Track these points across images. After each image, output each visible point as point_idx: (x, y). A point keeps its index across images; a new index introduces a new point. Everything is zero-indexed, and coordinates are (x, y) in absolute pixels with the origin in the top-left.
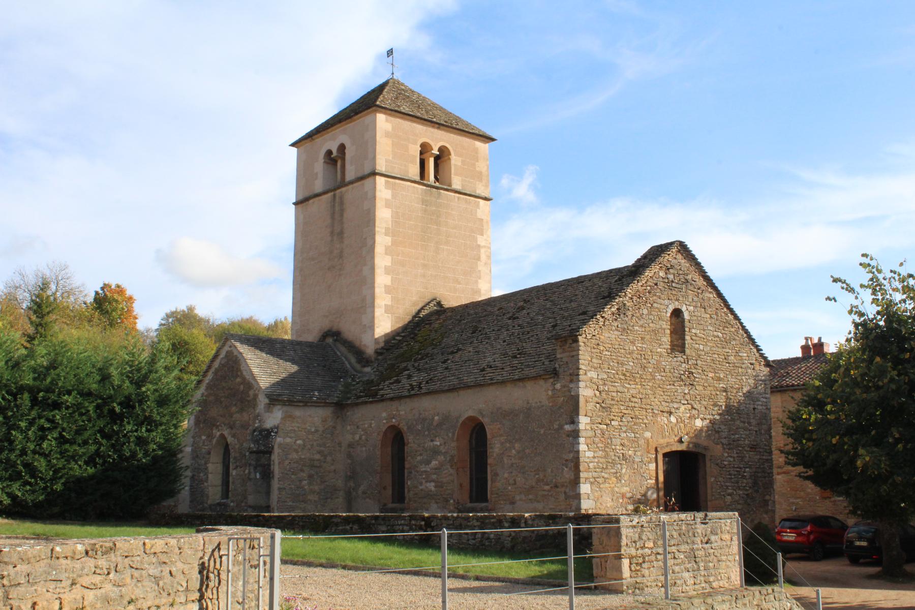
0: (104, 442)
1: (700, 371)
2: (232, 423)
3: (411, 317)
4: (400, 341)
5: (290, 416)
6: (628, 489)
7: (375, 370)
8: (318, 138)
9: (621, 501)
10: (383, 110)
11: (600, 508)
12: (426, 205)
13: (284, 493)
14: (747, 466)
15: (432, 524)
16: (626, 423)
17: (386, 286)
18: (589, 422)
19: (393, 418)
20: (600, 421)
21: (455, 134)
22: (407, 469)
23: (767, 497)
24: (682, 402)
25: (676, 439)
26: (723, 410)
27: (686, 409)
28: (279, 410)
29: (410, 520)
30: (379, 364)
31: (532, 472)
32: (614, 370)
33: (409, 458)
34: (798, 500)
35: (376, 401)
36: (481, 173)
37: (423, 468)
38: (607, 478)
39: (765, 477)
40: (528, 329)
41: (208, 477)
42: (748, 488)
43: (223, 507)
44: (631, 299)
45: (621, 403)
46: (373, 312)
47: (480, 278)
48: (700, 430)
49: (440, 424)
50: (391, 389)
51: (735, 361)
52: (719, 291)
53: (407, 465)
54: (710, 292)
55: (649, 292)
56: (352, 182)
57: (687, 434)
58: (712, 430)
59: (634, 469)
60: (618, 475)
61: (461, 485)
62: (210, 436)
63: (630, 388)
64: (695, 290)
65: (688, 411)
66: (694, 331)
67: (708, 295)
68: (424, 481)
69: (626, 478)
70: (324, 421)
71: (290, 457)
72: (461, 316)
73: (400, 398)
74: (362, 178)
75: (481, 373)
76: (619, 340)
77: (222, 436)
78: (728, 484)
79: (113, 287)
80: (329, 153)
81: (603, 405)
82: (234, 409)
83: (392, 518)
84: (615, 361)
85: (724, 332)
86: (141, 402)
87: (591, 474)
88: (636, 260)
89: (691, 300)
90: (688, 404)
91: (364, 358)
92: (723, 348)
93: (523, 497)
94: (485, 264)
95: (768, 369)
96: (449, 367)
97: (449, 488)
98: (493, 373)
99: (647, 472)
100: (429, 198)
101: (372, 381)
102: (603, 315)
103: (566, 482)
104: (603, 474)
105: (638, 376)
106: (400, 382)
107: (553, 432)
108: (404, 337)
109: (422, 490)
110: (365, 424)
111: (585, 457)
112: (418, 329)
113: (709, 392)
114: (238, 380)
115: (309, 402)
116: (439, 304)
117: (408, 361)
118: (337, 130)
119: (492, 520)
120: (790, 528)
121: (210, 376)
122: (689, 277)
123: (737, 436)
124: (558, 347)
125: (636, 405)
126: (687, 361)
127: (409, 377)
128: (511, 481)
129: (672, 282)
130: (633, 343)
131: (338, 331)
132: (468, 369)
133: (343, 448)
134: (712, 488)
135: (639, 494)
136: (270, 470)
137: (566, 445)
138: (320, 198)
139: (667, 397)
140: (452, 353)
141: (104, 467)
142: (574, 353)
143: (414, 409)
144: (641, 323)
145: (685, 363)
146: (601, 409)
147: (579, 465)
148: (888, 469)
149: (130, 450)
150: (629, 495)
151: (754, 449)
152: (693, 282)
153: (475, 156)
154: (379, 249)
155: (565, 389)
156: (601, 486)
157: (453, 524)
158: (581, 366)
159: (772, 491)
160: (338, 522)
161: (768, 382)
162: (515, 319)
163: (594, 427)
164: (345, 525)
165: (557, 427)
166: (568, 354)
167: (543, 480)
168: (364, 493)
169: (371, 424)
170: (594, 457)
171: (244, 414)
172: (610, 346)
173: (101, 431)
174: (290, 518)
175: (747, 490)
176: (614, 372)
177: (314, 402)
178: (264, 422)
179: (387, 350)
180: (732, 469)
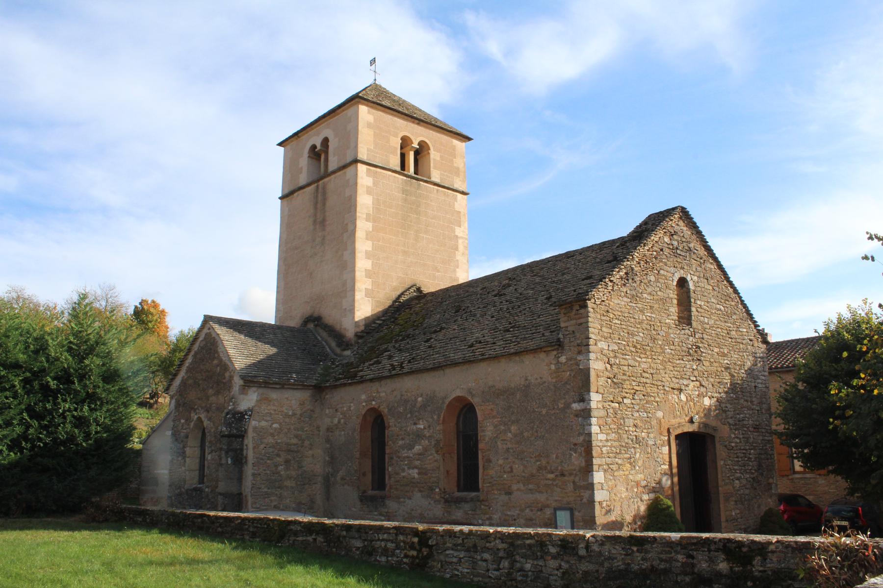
0: (35, 423)
2: (208, 406)
3: (391, 302)
4: (380, 324)
5: (266, 399)
7: (355, 353)
8: (304, 134)
9: (636, 490)
10: (366, 102)
12: (406, 195)
14: (752, 447)
15: (430, 543)
18: (601, 399)
19: (374, 400)
20: (612, 399)
22: (388, 454)
23: (771, 480)
24: (692, 378)
25: (687, 419)
26: (729, 388)
27: (694, 386)
28: (255, 392)
29: (397, 535)
30: (359, 347)
31: (531, 458)
32: (625, 341)
33: (390, 442)
35: (355, 383)
36: (458, 169)
37: (405, 453)
38: (621, 465)
39: (768, 459)
40: (519, 303)
41: (185, 461)
42: (753, 471)
43: (198, 492)
44: (639, 263)
45: (633, 378)
46: (354, 295)
47: (458, 268)
49: (424, 406)
50: (371, 370)
51: (737, 336)
52: (719, 262)
53: (387, 451)
55: (656, 258)
56: (334, 172)
58: (719, 410)
60: (632, 461)
61: (448, 472)
62: (188, 420)
63: (641, 362)
64: (698, 259)
65: (696, 389)
66: (699, 302)
67: (709, 265)
68: (406, 468)
69: (640, 463)
70: (302, 404)
71: (266, 441)
72: (442, 299)
73: (380, 379)
74: (344, 167)
75: (469, 349)
76: (628, 307)
77: (199, 419)
78: (736, 467)
79: (149, 302)
80: (314, 147)
81: (614, 380)
82: (211, 391)
83: (371, 530)
84: (625, 331)
86: (82, 378)
88: (635, 227)
89: (694, 270)
90: (697, 381)
91: (344, 342)
92: (725, 322)
93: (521, 486)
94: (463, 254)
95: (765, 346)
96: (433, 346)
97: (434, 475)
98: (484, 348)
99: (661, 456)
100: (409, 188)
101: (352, 363)
102: (611, 279)
103: (575, 470)
104: (617, 459)
105: (649, 348)
106: (380, 363)
107: (558, 411)
108: (384, 321)
109: (404, 477)
110: (344, 407)
111: (597, 440)
112: (398, 314)
114: (215, 362)
115: (285, 384)
116: (419, 290)
117: (389, 343)
118: (321, 126)
119: (528, 542)
121: (190, 360)
122: (692, 245)
124: (562, 315)
125: (648, 381)
126: (693, 335)
127: (390, 357)
128: (507, 469)
129: (677, 248)
130: (642, 311)
131: (319, 316)
132: (454, 346)
133: (321, 433)
135: (653, 482)
136: (242, 455)
137: (574, 426)
139: (677, 373)
140: (435, 332)
141: (32, 453)
142: (582, 320)
143: (395, 390)
144: (649, 290)
145: (692, 336)
146: (612, 384)
147: (591, 450)
149: (66, 433)
150: (644, 483)
152: (696, 251)
153: (453, 153)
154: (360, 234)
155: (571, 362)
156: (616, 474)
157: (463, 545)
158: (591, 335)
160: (297, 531)
161: (765, 360)
162: (501, 295)
163: (606, 404)
164: (307, 536)
165: (562, 406)
166: (573, 322)
167: (546, 468)
168: (343, 479)
169: (350, 407)
170: (607, 441)
171: (220, 396)
172: (620, 314)
173: (30, 410)
174: (240, 521)
175: (753, 473)
176: (624, 343)
177: (294, 385)
178: (238, 405)
179: (367, 333)
180: (739, 451)
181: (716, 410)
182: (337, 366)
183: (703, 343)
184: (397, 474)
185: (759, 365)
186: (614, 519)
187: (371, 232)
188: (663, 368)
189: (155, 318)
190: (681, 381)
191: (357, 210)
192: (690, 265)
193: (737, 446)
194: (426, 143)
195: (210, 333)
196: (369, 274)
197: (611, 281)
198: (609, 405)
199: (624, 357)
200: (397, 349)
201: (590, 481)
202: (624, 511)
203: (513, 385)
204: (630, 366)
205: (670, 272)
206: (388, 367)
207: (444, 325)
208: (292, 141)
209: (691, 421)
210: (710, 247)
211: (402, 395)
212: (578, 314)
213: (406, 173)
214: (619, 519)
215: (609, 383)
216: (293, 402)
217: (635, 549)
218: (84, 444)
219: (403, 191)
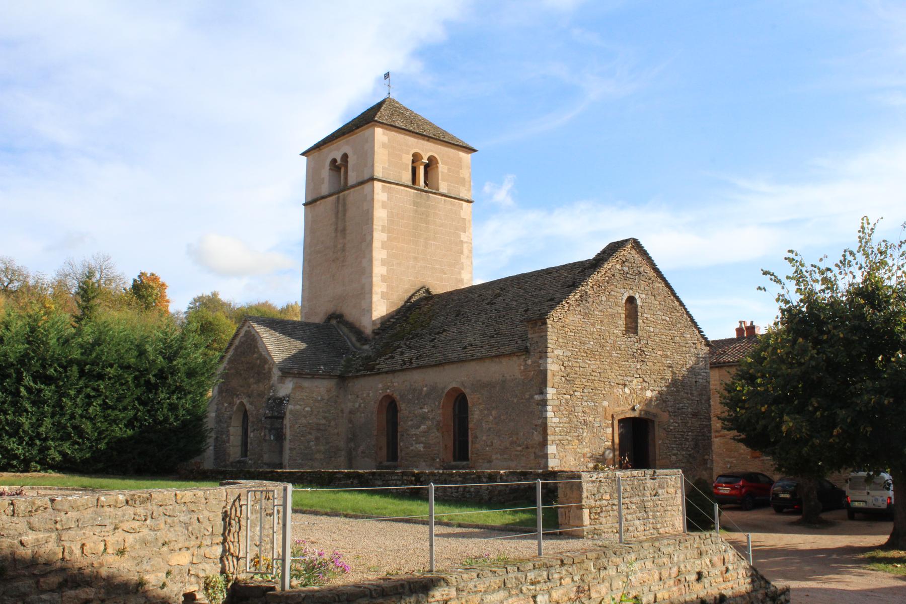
0: (141, 408)
1: (650, 350)
4: (394, 322)
8: (325, 148)
9: (582, 460)
10: (381, 125)
12: (417, 207)
15: (421, 479)
18: (555, 392)
19: (388, 389)
23: (706, 457)
24: (635, 376)
25: (630, 407)
26: (670, 383)
27: (638, 382)
28: (290, 381)
29: (402, 476)
33: (402, 423)
37: (413, 431)
38: (571, 441)
39: (704, 440)
40: (504, 313)
44: (592, 287)
46: (371, 298)
47: (463, 270)
51: (680, 341)
53: (399, 429)
55: (607, 282)
56: (353, 187)
58: (659, 400)
59: (594, 433)
61: (446, 446)
62: (231, 404)
65: (639, 384)
66: (645, 315)
68: (414, 443)
70: (329, 391)
71: (300, 421)
73: (393, 372)
76: (581, 322)
77: (242, 404)
78: (674, 446)
79: (148, 275)
81: (567, 378)
82: (252, 380)
84: (578, 341)
89: (643, 289)
91: (363, 337)
93: (498, 456)
99: (605, 435)
103: (535, 444)
105: (598, 353)
106: (394, 358)
108: (397, 319)
109: (412, 450)
111: (552, 422)
115: (316, 375)
116: (428, 291)
119: (472, 476)
120: (725, 483)
121: (231, 352)
122: (642, 269)
123: (681, 405)
125: (596, 378)
126: (639, 341)
127: (402, 353)
128: (489, 443)
129: (627, 273)
130: (593, 325)
136: (283, 432)
138: (326, 199)
140: (439, 333)
142: (543, 334)
144: (600, 308)
146: (566, 382)
148: (808, 433)
149: (164, 415)
150: (589, 455)
153: (459, 164)
154: (376, 244)
158: (549, 345)
161: (707, 359)
162: (492, 304)
163: (560, 397)
166: (537, 335)
167: (516, 442)
169: (369, 394)
170: (560, 423)
172: (573, 328)
175: (689, 451)
177: (321, 375)
179: (383, 330)
181: (657, 400)
182: (358, 359)
183: (647, 348)
184: (407, 448)
185: (701, 364)
187: (385, 242)
188: (609, 368)
189: (155, 292)
191: (374, 223)
192: (639, 286)
193: (674, 429)
194: (435, 157)
195: (249, 330)
196: (384, 279)
197: (568, 303)
199: (576, 360)
200: (407, 346)
201: (545, 452)
203: (494, 380)
205: (620, 293)
206: (400, 362)
207: (446, 327)
208: (314, 153)
209: (633, 409)
210: (658, 269)
211: (411, 385)
212: (540, 329)
213: (416, 187)
217: (522, 477)
218: (175, 424)
219: (414, 204)
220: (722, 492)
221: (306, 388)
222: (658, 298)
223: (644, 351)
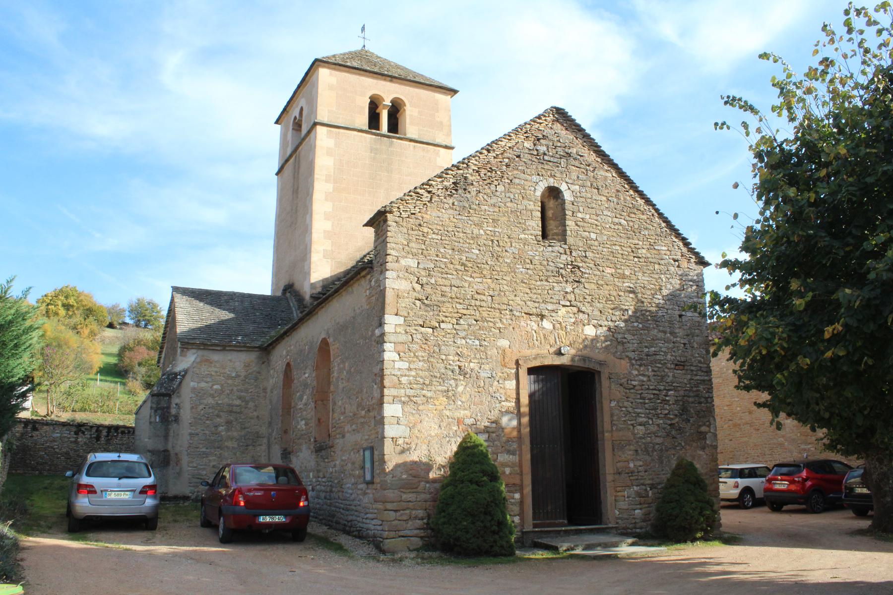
1: (592, 265)
6: (467, 413)
9: (455, 428)
11: (417, 437)
12: (376, 154)
13: (196, 439)
16: (467, 327)
17: (325, 231)
18: (402, 322)
20: (422, 323)
21: (410, 86)
23: (704, 429)
25: (552, 350)
27: (568, 312)
28: (194, 354)
32: (446, 258)
34: (809, 446)
36: (441, 123)
38: (431, 398)
39: (700, 403)
42: (672, 416)
45: (458, 300)
48: (592, 340)
51: (649, 255)
54: (607, 171)
55: (507, 166)
57: (570, 345)
58: (611, 341)
59: (479, 387)
61: (319, 420)
65: (572, 315)
66: (579, 215)
70: (247, 366)
71: (205, 402)
76: (455, 220)
81: (426, 301)
85: (630, 219)
87: (403, 391)
90: (571, 306)
99: (502, 391)
100: (378, 147)
104: (424, 392)
113: (607, 292)
120: (781, 474)
122: (574, 151)
125: (483, 304)
130: (479, 225)
134: (612, 415)
135: (486, 421)
145: (565, 254)
146: (423, 307)
148: (785, 345)
151: (681, 367)
156: (421, 408)
159: (712, 421)
163: (412, 330)
170: (410, 369)
175: (672, 419)
176: (445, 260)
186: (416, 459)
190: (543, 305)
198: (416, 330)
202: (432, 451)
204: (454, 286)
208: (284, 117)
209: (559, 353)
210: (603, 151)
214: (424, 460)
215: (418, 305)
216: (238, 364)
220: (777, 487)
221: (216, 362)
222: (605, 192)
223: (579, 268)
